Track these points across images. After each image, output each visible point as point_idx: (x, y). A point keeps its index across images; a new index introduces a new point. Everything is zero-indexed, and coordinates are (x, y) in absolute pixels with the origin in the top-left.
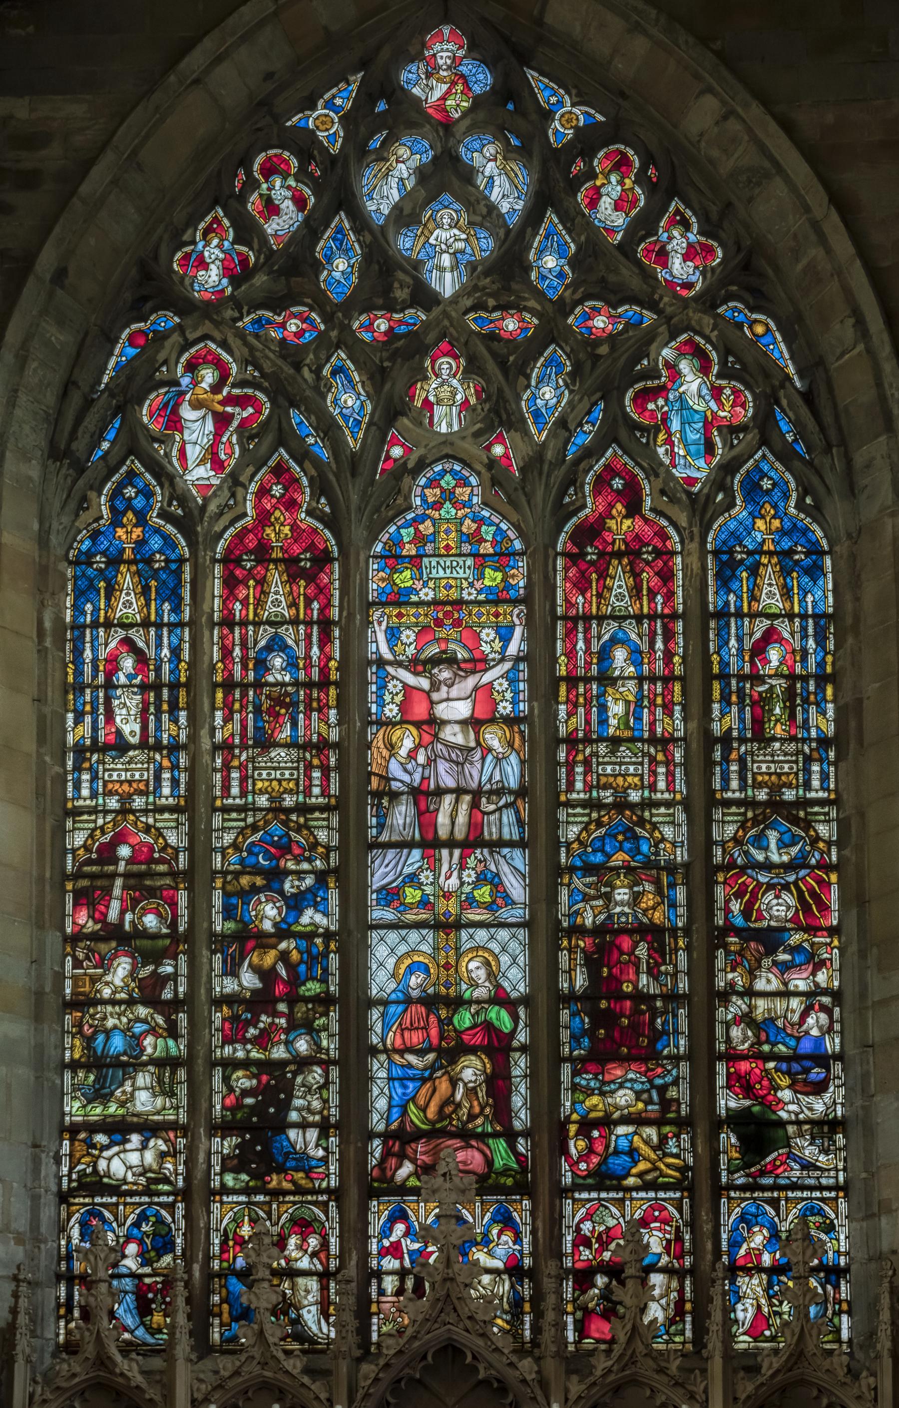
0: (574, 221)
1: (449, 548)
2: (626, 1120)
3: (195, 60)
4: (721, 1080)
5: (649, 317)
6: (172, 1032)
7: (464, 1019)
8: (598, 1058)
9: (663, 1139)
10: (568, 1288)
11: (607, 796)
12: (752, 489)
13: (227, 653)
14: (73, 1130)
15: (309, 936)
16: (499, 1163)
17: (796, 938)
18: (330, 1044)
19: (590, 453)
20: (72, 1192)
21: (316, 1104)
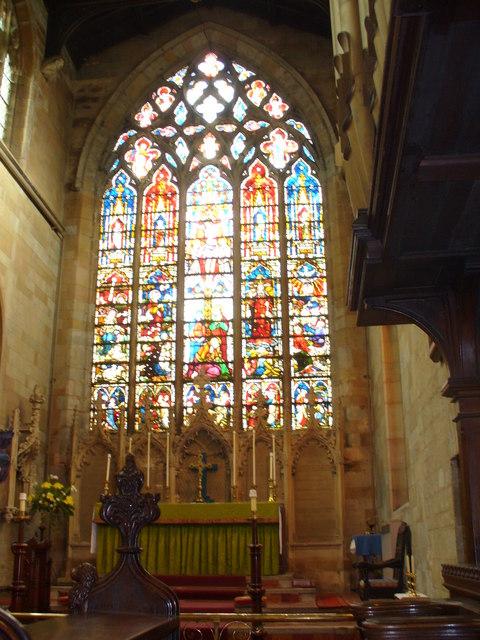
0: (246, 100)
1: (211, 187)
2: (262, 357)
3: (141, 66)
4: (291, 343)
5: (267, 125)
6: (126, 334)
7: (213, 327)
8: (254, 338)
9: (274, 362)
10: (244, 411)
11: (256, 258)
12: (297, 169)
13: (146, 221)
14: (96, 364)
15: (166, 303)
16: (223, 372)
17: (314, 299)
18: (173, 336)
19: (251, 162)
20: (95, 383)
21: (168, 355)
